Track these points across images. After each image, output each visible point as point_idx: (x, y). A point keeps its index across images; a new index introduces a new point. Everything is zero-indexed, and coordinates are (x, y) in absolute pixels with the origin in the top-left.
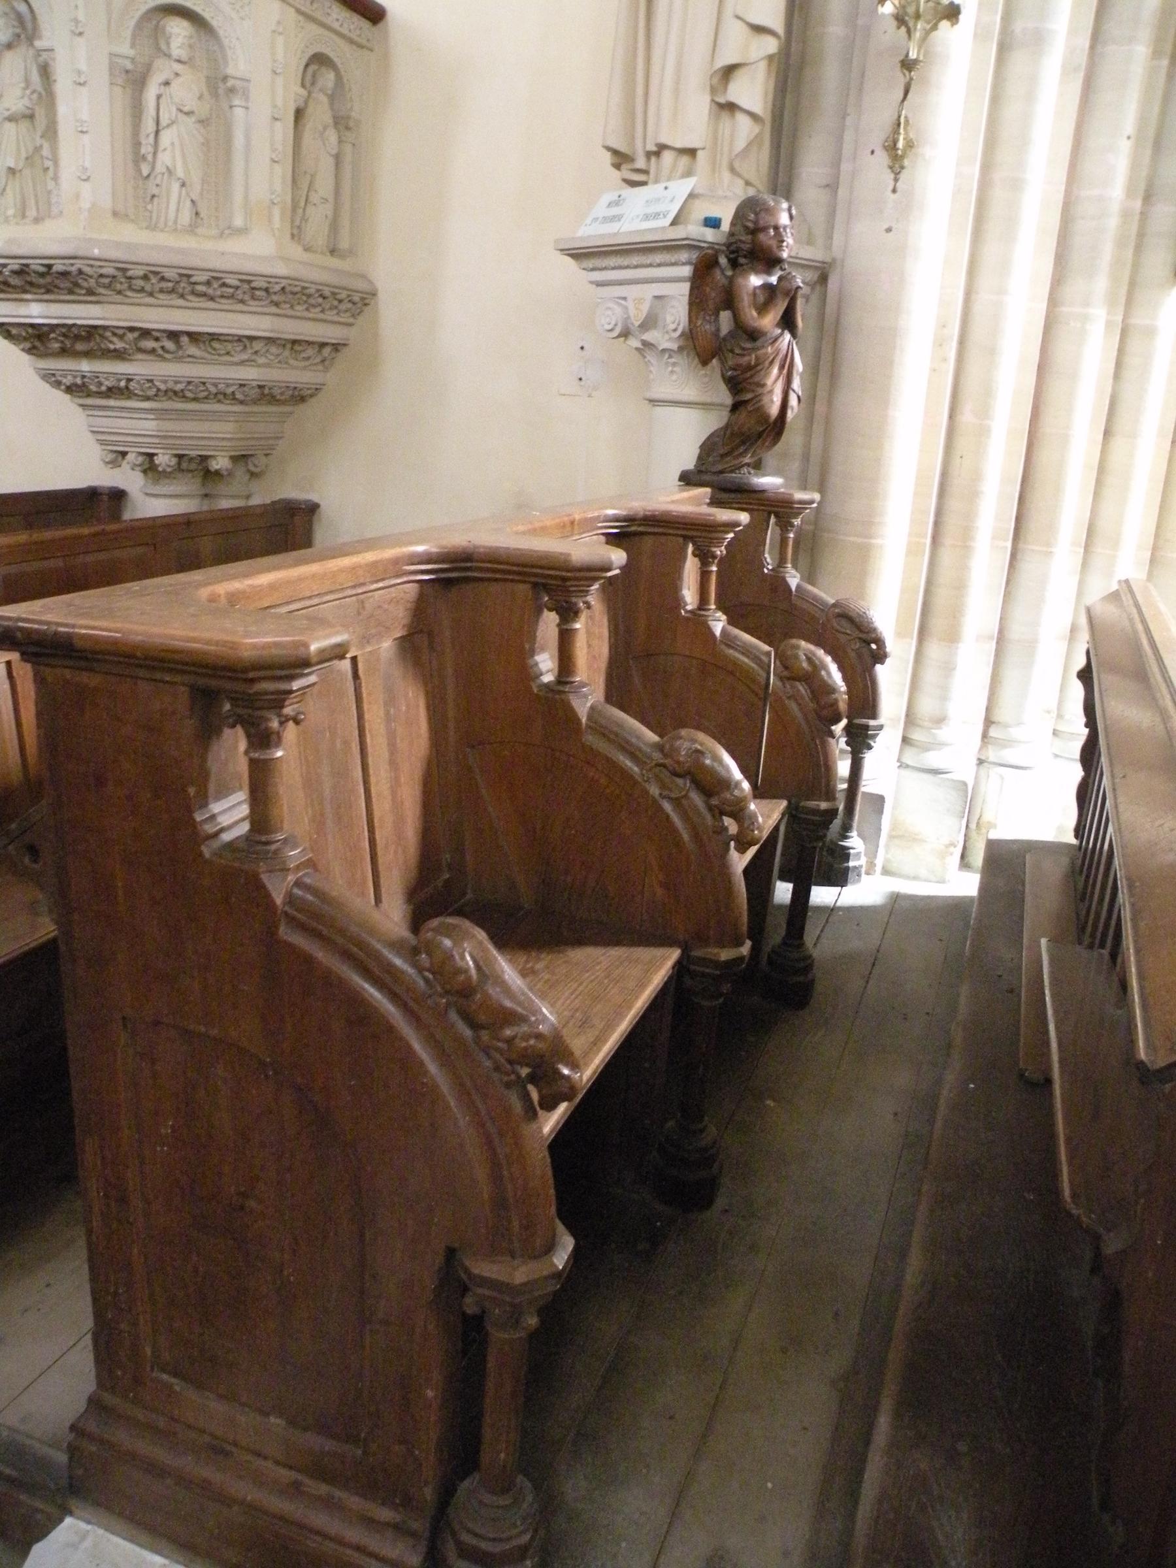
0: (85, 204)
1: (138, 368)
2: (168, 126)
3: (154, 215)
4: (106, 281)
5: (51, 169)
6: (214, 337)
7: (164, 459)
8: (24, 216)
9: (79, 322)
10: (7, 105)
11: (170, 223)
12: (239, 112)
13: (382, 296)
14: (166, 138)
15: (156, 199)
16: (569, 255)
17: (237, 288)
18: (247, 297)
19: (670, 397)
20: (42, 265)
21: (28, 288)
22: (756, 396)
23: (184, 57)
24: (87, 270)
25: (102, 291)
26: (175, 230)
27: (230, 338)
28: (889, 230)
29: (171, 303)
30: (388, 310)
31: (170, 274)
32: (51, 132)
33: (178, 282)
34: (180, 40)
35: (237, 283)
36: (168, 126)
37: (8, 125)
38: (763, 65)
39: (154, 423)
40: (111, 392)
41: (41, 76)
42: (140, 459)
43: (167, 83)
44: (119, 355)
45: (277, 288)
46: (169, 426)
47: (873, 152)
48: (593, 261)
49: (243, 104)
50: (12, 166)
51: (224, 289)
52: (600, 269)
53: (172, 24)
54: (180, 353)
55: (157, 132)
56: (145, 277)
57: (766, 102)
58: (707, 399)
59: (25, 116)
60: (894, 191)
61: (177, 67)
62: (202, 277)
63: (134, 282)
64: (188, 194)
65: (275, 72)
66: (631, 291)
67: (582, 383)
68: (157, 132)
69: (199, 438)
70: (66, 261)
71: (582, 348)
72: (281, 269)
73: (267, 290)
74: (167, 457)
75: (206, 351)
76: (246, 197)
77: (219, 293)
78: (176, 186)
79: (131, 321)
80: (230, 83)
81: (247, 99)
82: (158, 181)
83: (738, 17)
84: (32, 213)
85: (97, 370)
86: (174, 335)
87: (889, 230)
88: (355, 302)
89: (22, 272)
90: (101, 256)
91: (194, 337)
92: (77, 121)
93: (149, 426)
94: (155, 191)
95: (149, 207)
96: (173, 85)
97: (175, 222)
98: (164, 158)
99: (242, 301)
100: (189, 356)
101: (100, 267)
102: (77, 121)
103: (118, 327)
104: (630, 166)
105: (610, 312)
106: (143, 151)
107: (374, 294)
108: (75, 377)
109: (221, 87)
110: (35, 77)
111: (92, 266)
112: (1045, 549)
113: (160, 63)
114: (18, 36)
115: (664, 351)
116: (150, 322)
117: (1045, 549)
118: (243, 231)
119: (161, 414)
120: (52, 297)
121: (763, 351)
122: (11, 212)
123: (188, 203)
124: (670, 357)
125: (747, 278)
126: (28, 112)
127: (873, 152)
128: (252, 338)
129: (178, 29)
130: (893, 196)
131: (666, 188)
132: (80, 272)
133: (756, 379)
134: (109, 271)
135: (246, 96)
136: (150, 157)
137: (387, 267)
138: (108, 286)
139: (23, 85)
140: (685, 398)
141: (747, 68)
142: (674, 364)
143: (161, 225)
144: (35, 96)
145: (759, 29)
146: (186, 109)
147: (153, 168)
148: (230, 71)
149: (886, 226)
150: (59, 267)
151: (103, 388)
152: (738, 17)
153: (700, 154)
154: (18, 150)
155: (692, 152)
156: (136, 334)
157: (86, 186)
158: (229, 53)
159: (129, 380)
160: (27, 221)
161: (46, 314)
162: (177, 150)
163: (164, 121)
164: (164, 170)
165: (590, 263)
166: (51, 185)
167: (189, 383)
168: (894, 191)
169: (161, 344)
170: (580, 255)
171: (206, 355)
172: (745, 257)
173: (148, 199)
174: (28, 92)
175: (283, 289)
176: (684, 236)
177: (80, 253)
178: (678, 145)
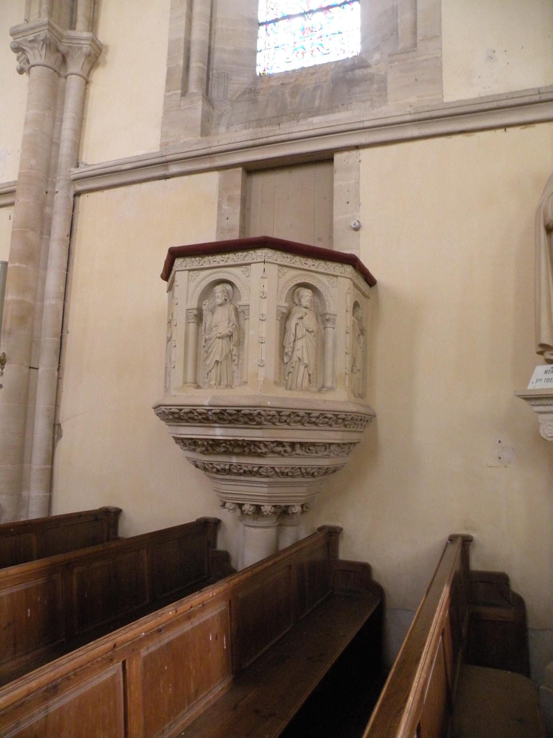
0: (261, 379)
1: (267, 462)
2: (301, 338)
3: (289, 382)
4: (269, 418)
5: (236, 361)
6: (314, 444)
7: (267, 508)
8: (220, 384)
9: (246, 439)
10: (220, 331)
11: (299, 386)
12: (330, 330)
13: (378, 417)
14: (300, 343)
15: (290, 374)
17: (330, 419)
18: (333, 423)
20: (235, 410)
21: (218, 421)
23: (309, 306)
24: (263, 413)
25: (265, 423)
26: (302, 390)
27: (321, 444)
29: (311, 428)
30: (383, 425)
31: (302, 413)
32: (240, 343)
33: (303, 417)
34: (308, 298)
35: (332, 416)
36: (301, 338)
37: (218, 340)
39: (266, 489)
40: (251, 473)
41: (235, 316)
42: (252, 508)
43: (302, 318)
44: (261, 455)
45: (350, 418)
46: (277, 491)
49: (332, 326)
50: (218, 360)
51: (324, 419)
53: (304, 291)
54: (293, 453)
55: (295, 341)
56: (289, 416)
57: (67, 320)
59: (227, 336)
61: (305, 310)
62: (316, 414)
63: (282, 417)
64: (308, 371)
65: (347, 311)
67: (501, 460)
68: (295, 341)
69: (290, 496)
70: (249, 408)
72: (352, 408)
73: (344, 420)
74: (270, 507)
75: (306, 452)
76: (333, 372)
77: (321, 422)
78: (302, 368)
79: (275, 438)
80: (327, 317)
81: (334, 324)
82: (294, 365)
84: (224, 382)
85: (241, 462)
86: (293, 445)
88: (362, 421)
89: (222, 412)
90: (272, 406)
91: (302, 444)
92: (260, 338)
93: (263, 490)
94: (291, 370)
95: (286, 378)
96: (304, 319)
97: (302, 385)
98: (297, 354)
99: (331, 426)
100: (297, 454)
101: (270, 411)
102: (260, 338)
103: (267, 441)
106: (286, 350)
107: (375, 416)
108: (226, 465)
109: (323, 319)
110: (233, 317)
111: (265, 411)
113: (295, 309)
114: (226, 300)
116: (285, 438)
118: (331, 389)
119: (270, 485)
120: (232, 425)
122: (213, 382)
123: (307, 376)
126: (230, 334)
128: (330, 444)
129: (306, 294)
132: (259, 414)
134: (273, 413)
135: (334, 322)
136: (290, 354)
137: (381, 403)
138: (270, 421)
139: (228, 322)
143: (294, 386)
144: (234, 326)
146: (310, 330)
147: (291, 359)
148: (328, 311)
150: (246, 411)
151: (242, 471)
154: (222, 351)
156: (275, 444)
157: (262, 369)
158: (327, 303)
159: (260, 468)
160: (221, 386)
161: (224, 434)
162: (303, 349)
163: (299, 335)
164: (297, 359)
165: (533, 402)
166: (235, 368)
167: (293, 468)
169: (285, 449)
171: (306, 454)
173: (287, 374)
174: (231, 324)
175: (352, 418)
177: (262, 404)
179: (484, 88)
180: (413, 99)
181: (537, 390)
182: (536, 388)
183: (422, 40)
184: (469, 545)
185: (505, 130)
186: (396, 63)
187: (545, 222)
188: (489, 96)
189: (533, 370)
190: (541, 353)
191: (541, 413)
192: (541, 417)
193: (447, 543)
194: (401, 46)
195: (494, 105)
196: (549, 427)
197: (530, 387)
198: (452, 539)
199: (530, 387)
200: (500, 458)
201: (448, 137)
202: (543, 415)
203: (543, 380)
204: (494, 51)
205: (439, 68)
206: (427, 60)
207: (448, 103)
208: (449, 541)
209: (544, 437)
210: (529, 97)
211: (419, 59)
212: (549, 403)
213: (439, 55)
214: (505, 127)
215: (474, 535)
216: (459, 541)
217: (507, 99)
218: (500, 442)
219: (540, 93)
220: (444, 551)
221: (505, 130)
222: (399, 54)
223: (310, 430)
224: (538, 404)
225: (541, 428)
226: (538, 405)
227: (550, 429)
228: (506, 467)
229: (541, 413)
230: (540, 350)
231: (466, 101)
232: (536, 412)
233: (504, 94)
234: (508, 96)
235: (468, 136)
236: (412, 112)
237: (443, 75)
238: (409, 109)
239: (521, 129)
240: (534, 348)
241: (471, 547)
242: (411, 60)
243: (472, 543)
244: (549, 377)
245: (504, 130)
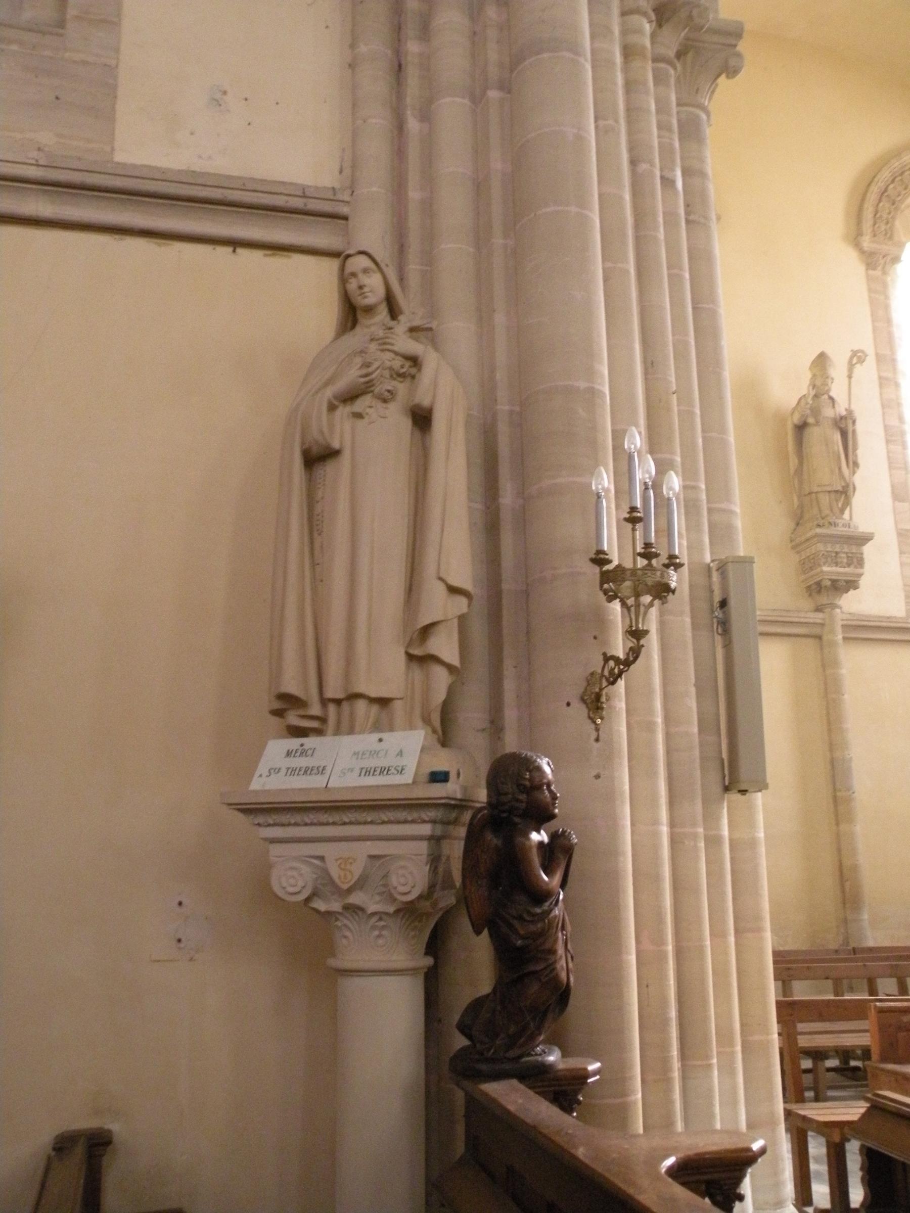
16: (239, 810)
19: (383, 966)
22: (551, 964)
28: (598, 777)
38: (456, 621)
47: (568, 704)
48: (274, 817)
52: (283, 825)
58: (411, 964)
60: (597, 740)
66: (329, 850)
67: (182, 945)
71: (180, 904)
83: (441, 579)
87: (598, 777)
104: (301, 712)
105: (295, 873)
112: (704, 1063)
115: (374, 914)
117: (704, 1063)
121: (552, 915)
124: (380, 919)
125: (526, 835)
127: (568, 704)
130: (597, 745)
131: (380, 740)
133: (547, 946)
140: (399, 965)
141: (441, 627)
142: (383, 927)
145: (454, 590)
149: (594, 773)
152: (441, 579)
153: (398, 705)
155: (384, 702)
165: (261, 819)
168: (597, 740)
170: (249, 810)
172: (519, 816)
176: (444, 795)
178: (373, 695)
179: (200, 157)
180: (46, 138)
181: (268, 792)
182: (267, 788)
183: (77, 18)
184: (101, 1156)
185: (234, 251)
186: (14, 47)
187: (303, 443)
188: (209, 174)
189: (263, 747)
190: (278, 713)
191: (273, 841)
192: (276, 850)
193: (49, 1158)
194: (27, 15)
195: (216, 194)
196: (290, 873)
197: (256, 785)
198: (63, 1145)
199: (256, 785)
200: (179, 941)
201: (117, 237)
202: (277, 846)
203: (283, 771)
204: (225, 93)
205: (111, 90)
206: (85, 63)
207: (124, 165)
208: (53, 1153)
209: (280, 893)
210: (286, 198)
211: (67, 55)
212: (331, 820)
213: (113, 63)
214: (235, 243)
215: (115, 1127)
216: (79, 1151)
217: (242, 190)
218: (180, 904)
219: (304, 196)
220: (43, 1185)
221: (234, 251)
222: (23, 29)
223: (443, 520)
224: (347, 820)
225: (275, 874)
226: (306, 824)
227: (293, 877)
228: (191, 960)
229: (273, 841)
230: (277, 705)
231: (163, 171)
232: (265, 839)
233: (240, 178)
234: (245, 184)
235: (159, 245)
236: (41, 162)
237: (117, 107)
238: (35, 154)
239: (265, 255)
240: (267, 702)
241: (105, 1160)
242: (47, 53)
243: (111, 1147)
244: (293, 765)
245: (230, 249)
